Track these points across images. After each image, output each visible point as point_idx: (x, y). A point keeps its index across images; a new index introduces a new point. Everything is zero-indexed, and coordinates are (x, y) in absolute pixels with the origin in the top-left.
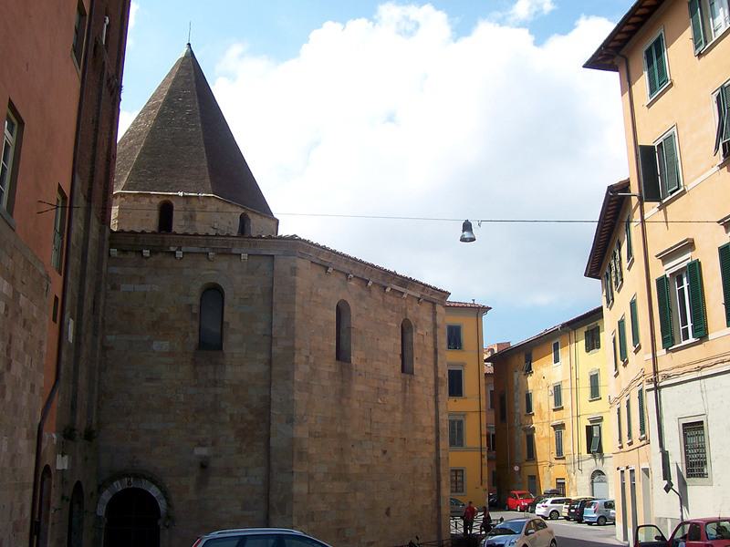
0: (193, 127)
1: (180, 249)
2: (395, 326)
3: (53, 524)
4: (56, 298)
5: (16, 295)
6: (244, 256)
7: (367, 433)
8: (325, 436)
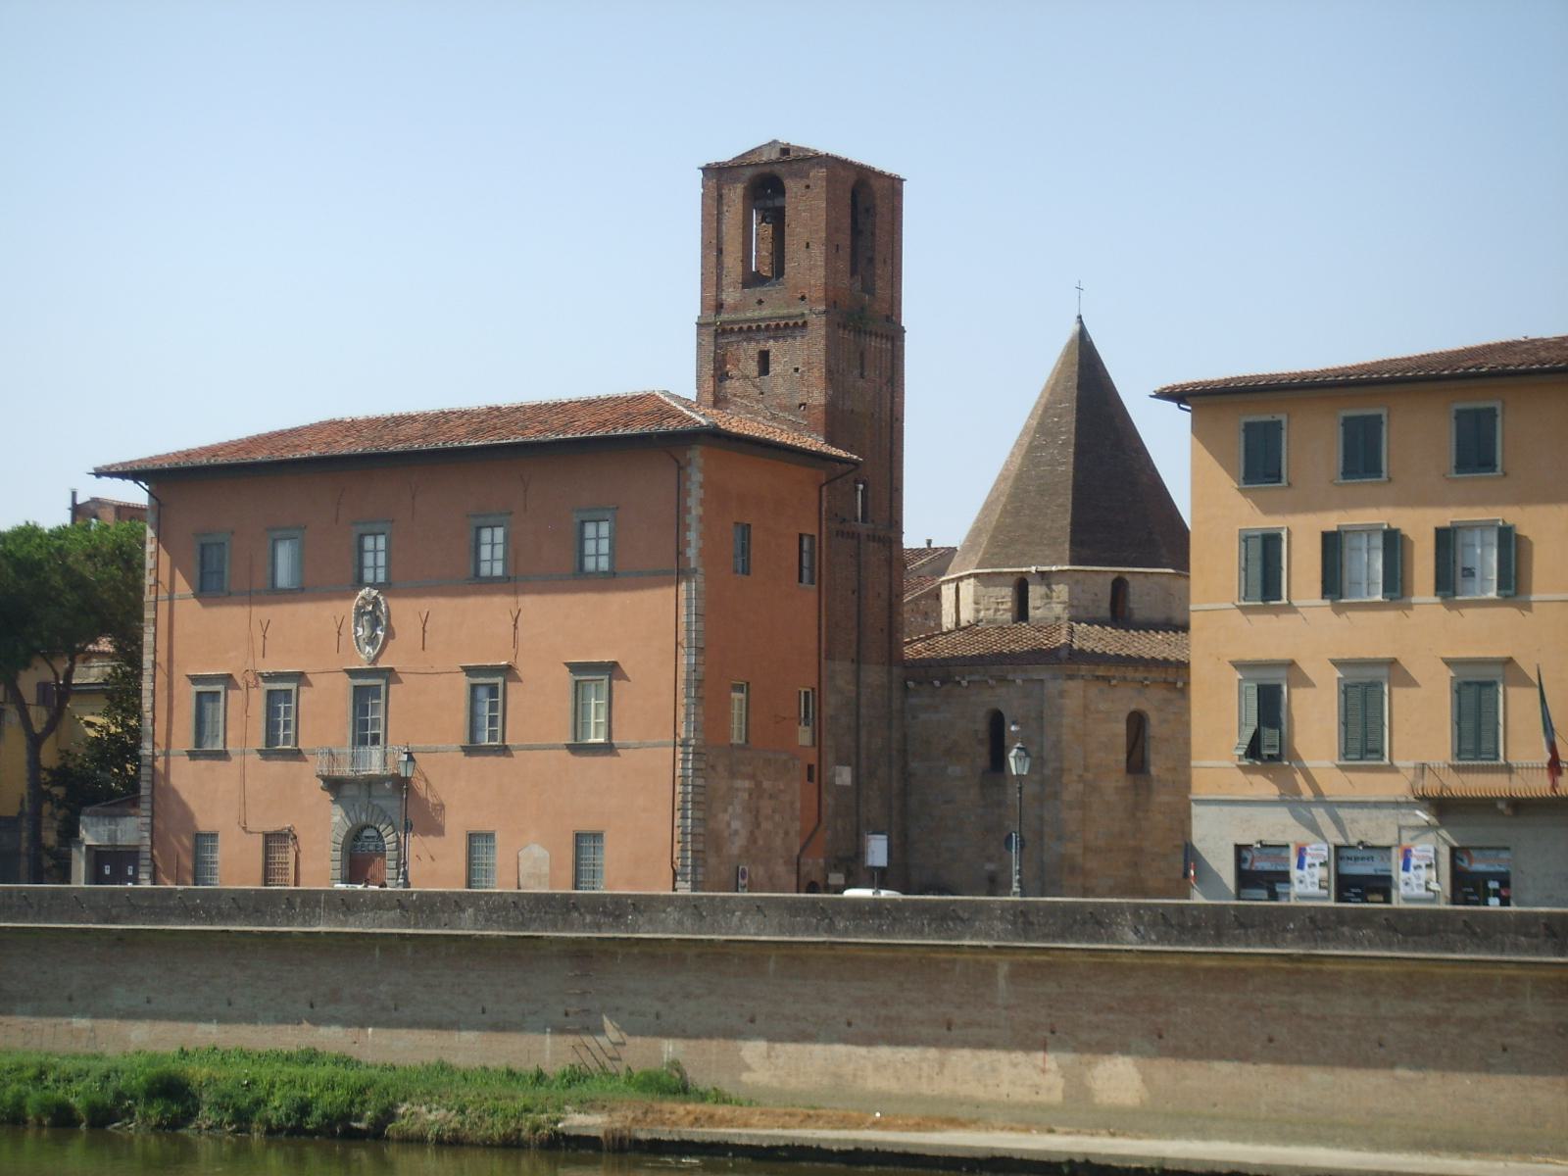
0: (1064, 463)
1: (964, 678)
3: (784, 1127)
4: (810, 768)
5: (758, 784)
6: (1019, 681)
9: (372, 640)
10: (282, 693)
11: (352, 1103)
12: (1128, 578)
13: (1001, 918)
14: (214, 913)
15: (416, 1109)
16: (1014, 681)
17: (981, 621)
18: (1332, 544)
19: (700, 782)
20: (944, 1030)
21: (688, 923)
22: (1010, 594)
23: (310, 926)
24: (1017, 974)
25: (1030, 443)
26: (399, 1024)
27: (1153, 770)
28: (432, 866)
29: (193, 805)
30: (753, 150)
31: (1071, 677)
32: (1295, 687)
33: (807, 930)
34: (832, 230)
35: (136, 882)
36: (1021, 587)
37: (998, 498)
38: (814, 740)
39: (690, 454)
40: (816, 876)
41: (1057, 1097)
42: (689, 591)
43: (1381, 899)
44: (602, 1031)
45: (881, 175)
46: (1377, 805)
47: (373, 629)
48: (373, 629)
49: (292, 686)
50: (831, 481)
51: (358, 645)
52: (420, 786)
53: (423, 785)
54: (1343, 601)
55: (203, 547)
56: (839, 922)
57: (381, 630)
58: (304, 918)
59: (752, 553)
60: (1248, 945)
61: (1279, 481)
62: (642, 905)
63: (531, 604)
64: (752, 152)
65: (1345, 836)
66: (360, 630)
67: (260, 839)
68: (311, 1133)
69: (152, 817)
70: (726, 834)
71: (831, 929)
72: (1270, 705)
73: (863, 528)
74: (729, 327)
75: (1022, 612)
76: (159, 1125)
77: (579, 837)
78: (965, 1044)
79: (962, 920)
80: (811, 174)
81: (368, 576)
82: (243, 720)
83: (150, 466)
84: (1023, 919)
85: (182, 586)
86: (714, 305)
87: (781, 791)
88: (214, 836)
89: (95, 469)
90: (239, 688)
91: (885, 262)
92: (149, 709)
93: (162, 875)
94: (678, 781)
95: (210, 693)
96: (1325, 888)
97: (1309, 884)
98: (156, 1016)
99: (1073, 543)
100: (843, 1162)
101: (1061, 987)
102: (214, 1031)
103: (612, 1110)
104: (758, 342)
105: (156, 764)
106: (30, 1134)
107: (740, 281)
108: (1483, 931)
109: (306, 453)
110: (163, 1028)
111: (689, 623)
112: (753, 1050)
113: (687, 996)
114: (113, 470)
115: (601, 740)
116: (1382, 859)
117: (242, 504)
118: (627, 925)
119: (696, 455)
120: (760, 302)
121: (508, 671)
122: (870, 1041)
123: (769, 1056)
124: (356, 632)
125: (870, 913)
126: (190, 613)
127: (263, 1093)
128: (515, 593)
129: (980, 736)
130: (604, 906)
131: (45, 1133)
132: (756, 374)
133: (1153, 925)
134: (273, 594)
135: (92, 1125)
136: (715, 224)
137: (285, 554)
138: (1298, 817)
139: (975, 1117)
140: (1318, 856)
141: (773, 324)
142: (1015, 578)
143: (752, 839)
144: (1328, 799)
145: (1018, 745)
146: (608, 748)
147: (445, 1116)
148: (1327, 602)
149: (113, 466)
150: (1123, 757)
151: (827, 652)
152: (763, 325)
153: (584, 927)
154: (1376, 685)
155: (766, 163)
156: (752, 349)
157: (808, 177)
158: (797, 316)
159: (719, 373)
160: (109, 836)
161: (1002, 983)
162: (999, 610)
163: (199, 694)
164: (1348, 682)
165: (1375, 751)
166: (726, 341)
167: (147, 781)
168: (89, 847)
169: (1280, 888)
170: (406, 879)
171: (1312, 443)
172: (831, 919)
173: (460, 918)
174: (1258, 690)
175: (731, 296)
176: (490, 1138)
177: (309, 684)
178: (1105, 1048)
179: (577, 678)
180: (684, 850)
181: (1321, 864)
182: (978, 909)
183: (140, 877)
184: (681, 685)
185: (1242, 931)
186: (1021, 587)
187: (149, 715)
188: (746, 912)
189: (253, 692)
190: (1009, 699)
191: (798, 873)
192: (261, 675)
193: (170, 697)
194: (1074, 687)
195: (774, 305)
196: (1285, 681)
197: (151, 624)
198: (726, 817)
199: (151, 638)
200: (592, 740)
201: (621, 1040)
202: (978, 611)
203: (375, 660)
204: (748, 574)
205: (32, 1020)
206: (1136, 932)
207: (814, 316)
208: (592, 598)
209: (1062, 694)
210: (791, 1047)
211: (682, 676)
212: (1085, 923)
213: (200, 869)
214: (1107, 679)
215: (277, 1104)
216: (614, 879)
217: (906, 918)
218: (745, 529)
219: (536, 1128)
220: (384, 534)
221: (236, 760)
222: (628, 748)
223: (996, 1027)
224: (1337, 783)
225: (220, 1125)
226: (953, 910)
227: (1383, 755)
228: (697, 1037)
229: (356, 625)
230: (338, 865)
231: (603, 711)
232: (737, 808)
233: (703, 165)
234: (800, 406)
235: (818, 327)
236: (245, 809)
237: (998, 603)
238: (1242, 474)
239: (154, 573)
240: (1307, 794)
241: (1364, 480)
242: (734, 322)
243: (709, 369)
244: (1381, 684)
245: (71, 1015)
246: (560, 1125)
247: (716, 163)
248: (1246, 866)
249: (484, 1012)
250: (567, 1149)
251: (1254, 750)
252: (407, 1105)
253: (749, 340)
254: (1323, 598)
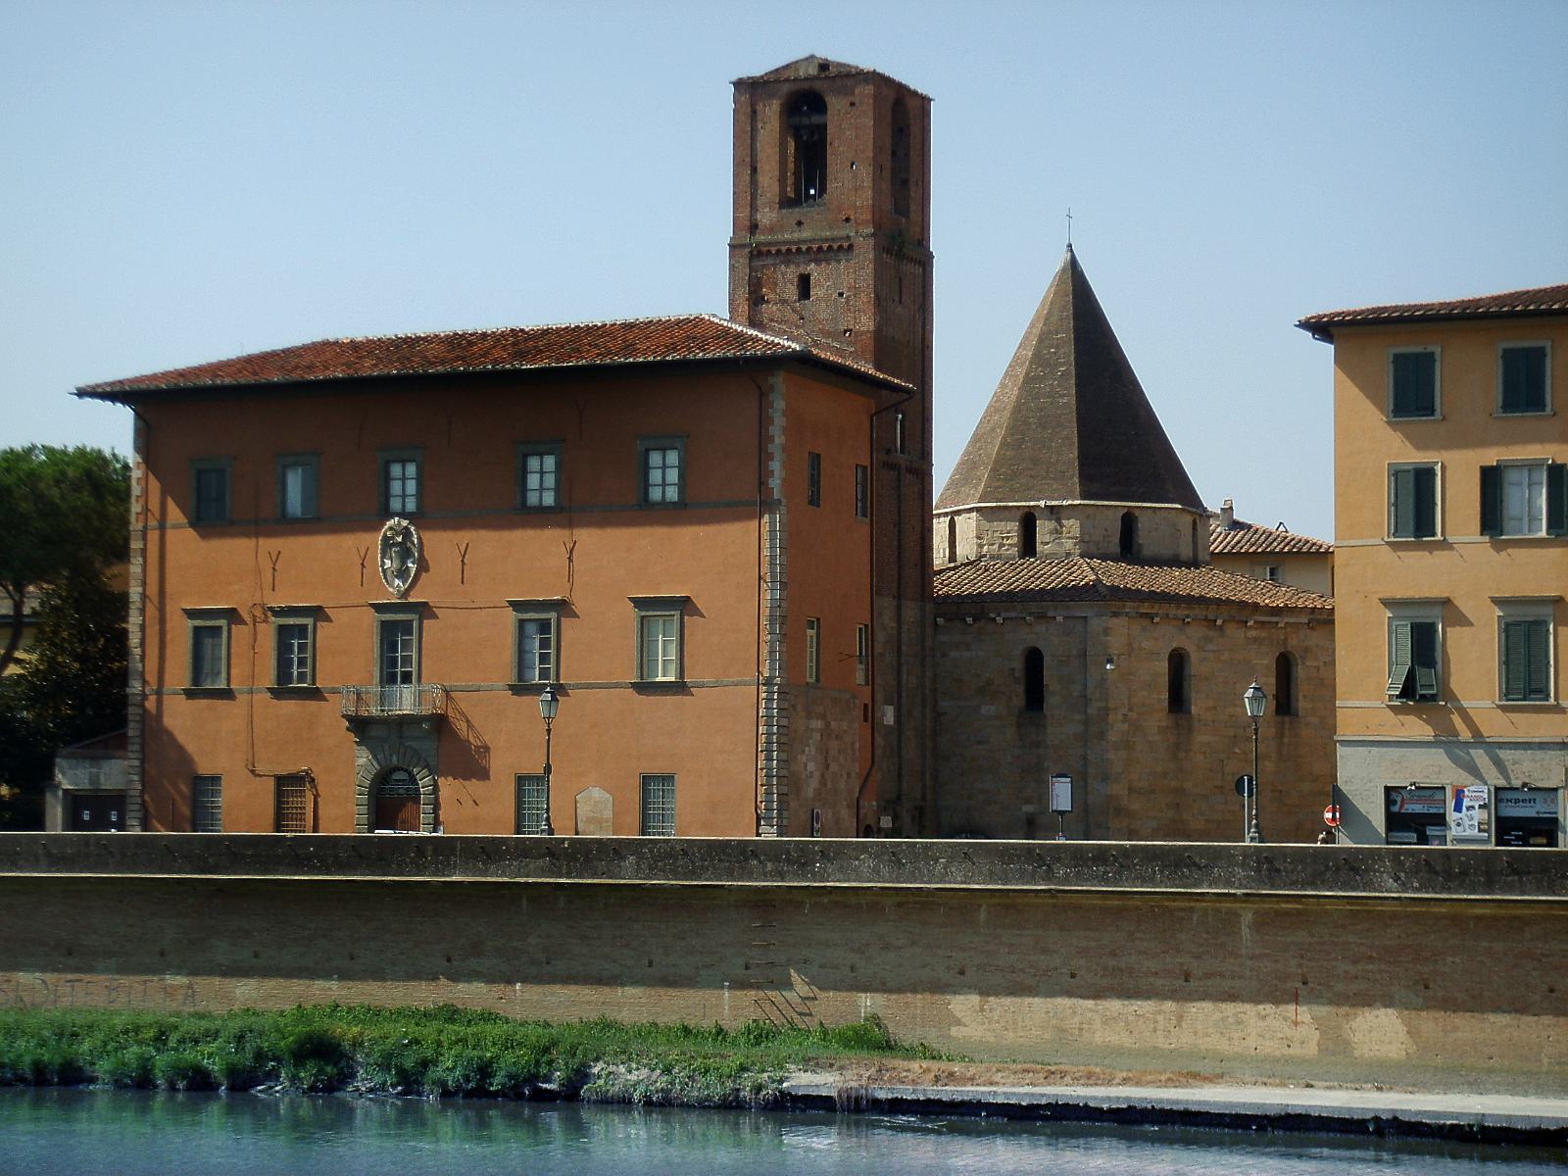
0: (1065, 395)
1: (999, 615)
2: (1266, 661)
4: (866, 705)
5: (828, 724)
6: (1059, 619)
7: (1216, 787)
8: (1153, 791)
9: (402, 573)
10: (295, 632)
11: (537, 1063)
12: (1137, 513)
13: (1243, 865)
14: (330, 862)
15: (612, 1068)
16: (1055, 618)
17: (985, 556)
18: (1492, 480)
19: (784, 722)
20: (1181, 982)
21: (885, 871)
22: (1016, 528)
23: (444, 875)
24: (1261, 924)
25: (1027, 374)
26: (553, 980)
27: (1194, 710)
28: (469, 810)
29: (191, 747)
30: (787, 65)
31: (1115, 615)
32: (1450, 626)
33: (1022, 879)
34: (878, 149)
35: (121, 826)
36: (1028, 522)
37: (993, 429)
38: (867, 677)
39: (772, 380)
40: (871, 821)
41: (1312, 1049)
42: (772, 523)
43: (1545, 841)
44: (788, 985)
45: (915, 93)
46: (1542, 746)
47: (403, 562)
48: (403, 562)
49: (309, 621)
50: (879, 412)
51: (385, 578)
52: (461, 727)
53: (464, 725)
54: (1503, 537)
55: (200, 473)
56: (1059, 869)
57: (413, 563)
58: (437, 867)
59: (822, 483)
60: (1523, 893)
61: (1432, 414)
62: (741, 855)
63: (587, 538)
64: (787, 66)
65: (1507, 778)
66: (388, 563)
67: (271, 784)
68: (495, 1095)
69: (143, 761)
70: (804, 776)
71: (1049, 877)
72: (1424, 645)
73: (902, 459)
74: (766, 249)
75: (1028, 546)
76: (313, 1088)
77: (646, 780)
78: (1206, 996)
79: (1199, 868)
80: (856, 92)
81: (395, 505)
82: (251, 657)
83: (143, 386)
84: (1268, 865)
85: (175, 513)
86: (747, 225)
87: (845, 732)
88: (215, 780)
89: (77, 389)
90: (245, 623)
91: (917, 185)
92: (138, 645)
93: (154, 821)
94: (762, 721)
95: (209, 630)
96: (1484, 831)
97: (1467, 826)
98: (265, 972)
99: (1082, 476)
100: (1114, 1121)
101: (1313, 936)
102: (335, 987)
103: (841, 1068)
104: (797, 265)
105: (147, 704)
106: (160, 1098)
107: (777, 201)
108: (1519, 871)
109: (330, 374)
110: (271, 985)
111: (773, 557)
112: (963, 1004)
113: (886, 947)
114: (100, 390)
115: (673, 679)
116: (1545, 801)
117: (263, 432)
118: (814, 874)
119: (779, 381)
120: (799, 223)
121: (563, 607)
122: (1098, 994)
123: (982, 1010)
124: (383, 564)
125: (1093, 859)
126: (185, 545)
127: (429, 1053)
128: (570, 524)
129: (1017, 675)
130: (788, 853)
131: (180, 1097)
132: (796, 297)
133: (1415, 871)
134: (284, 524)
135: (232, 1089)
136: (749, 141)
137: (294, 482)
138: (1457, 761)
139: (1219, 1071)
140: (1477, 798)
141: (815, 247)
142: (1021, 512)
143: (823, 782)
144: (1488, 740)
145: (1253, 685)
146: (680, 688)
147: (649, 1077)
148: (1487, 538)
149: (98, 386)
150: (1165, 696)
151: (875, 591)
152: (804, 248)
153: (765, 876)
154: (1541, 624)
155: (806, 79)
156: (790, 273)
157: (853, 94)
158: (841, 239)
159: (754, 296)
160: (90, 780)
161: (1245, 931)
162: (1004, 545)
163: (197, 629)
164: (1510, 620)
165: (1540, 691)
166: (762, 263)
167: (136, 721)
168: (66, 791)
169: (1431, 831)
170: (549, 825)
171: (1469, 377)
172: (1048, 866)
173: (620, 867)
174: (1412, 627)
175: (766, 216)
176: (708, 1098)
177: (328, 619)
178: (1365, 1000)
179: (643, 614)
180: (768, 793)
181: (1480, 807)
182: (1217, 855)
183: (128, 823)
184: (764, 622)
185: (1516, 878)
186: (1028, 522)
187: (138, 651)
188: (951, 859)
189: (261, 627)
190: (1051, 640)
191: (858, 818)
192: (271, 609)
193: (162, 633)
194: (1119, 624)
195: (813, 226)
196: (1440, 620)
197: (139, 553)
198: (804, 758)
199: (139, 570)
200: (660, 679)
201: (812, 995)
202: (981, 546)
203: (406, 593)
204: (818, 506)
205: (117, 977)
206: (1397, 879)
207: (861, 239)
208: (661, 532)
209: (1106, 631)
210: (1008, 1001)
211: (766, 612)
212: (1338, 869)
213: (201, 812)
214: (1150, 617)
215: (449, 1064)
216: (689, 821)
217: (1134, 865)
218: (815, 459)
219: (758, 1088)
220: (414, 461)
221: (242, 699)
222: (702, 686)
223: (1240, 977)
224: (1497, 724)
225: (383, 1087)
226: (1189, 856)
227: (1548, 695)
228: (899, 990)
229: (383, 557)
230: (364, 809)
231: (673, 650)
232: (811, 750)
233: (734, 79)
234: (845, 332)
235: (866, 252)
236: (248, 750)
237: (1003, 538)
238: (1391, 407)
239: (142, 501)
240: (1465, 735)
241: (1525, 414)
242: (769, 244)
243: (743, 292)
244: (1546, 623)
245: (163, 972)
246: (785, 1085)
247: (749, 78)
248: (1395, 809)
249: (650, 964)
250: (793, 1111)
251: (1408, 691)
252: (600, 1065)
253: (787, 263)
254: (1482, 535)
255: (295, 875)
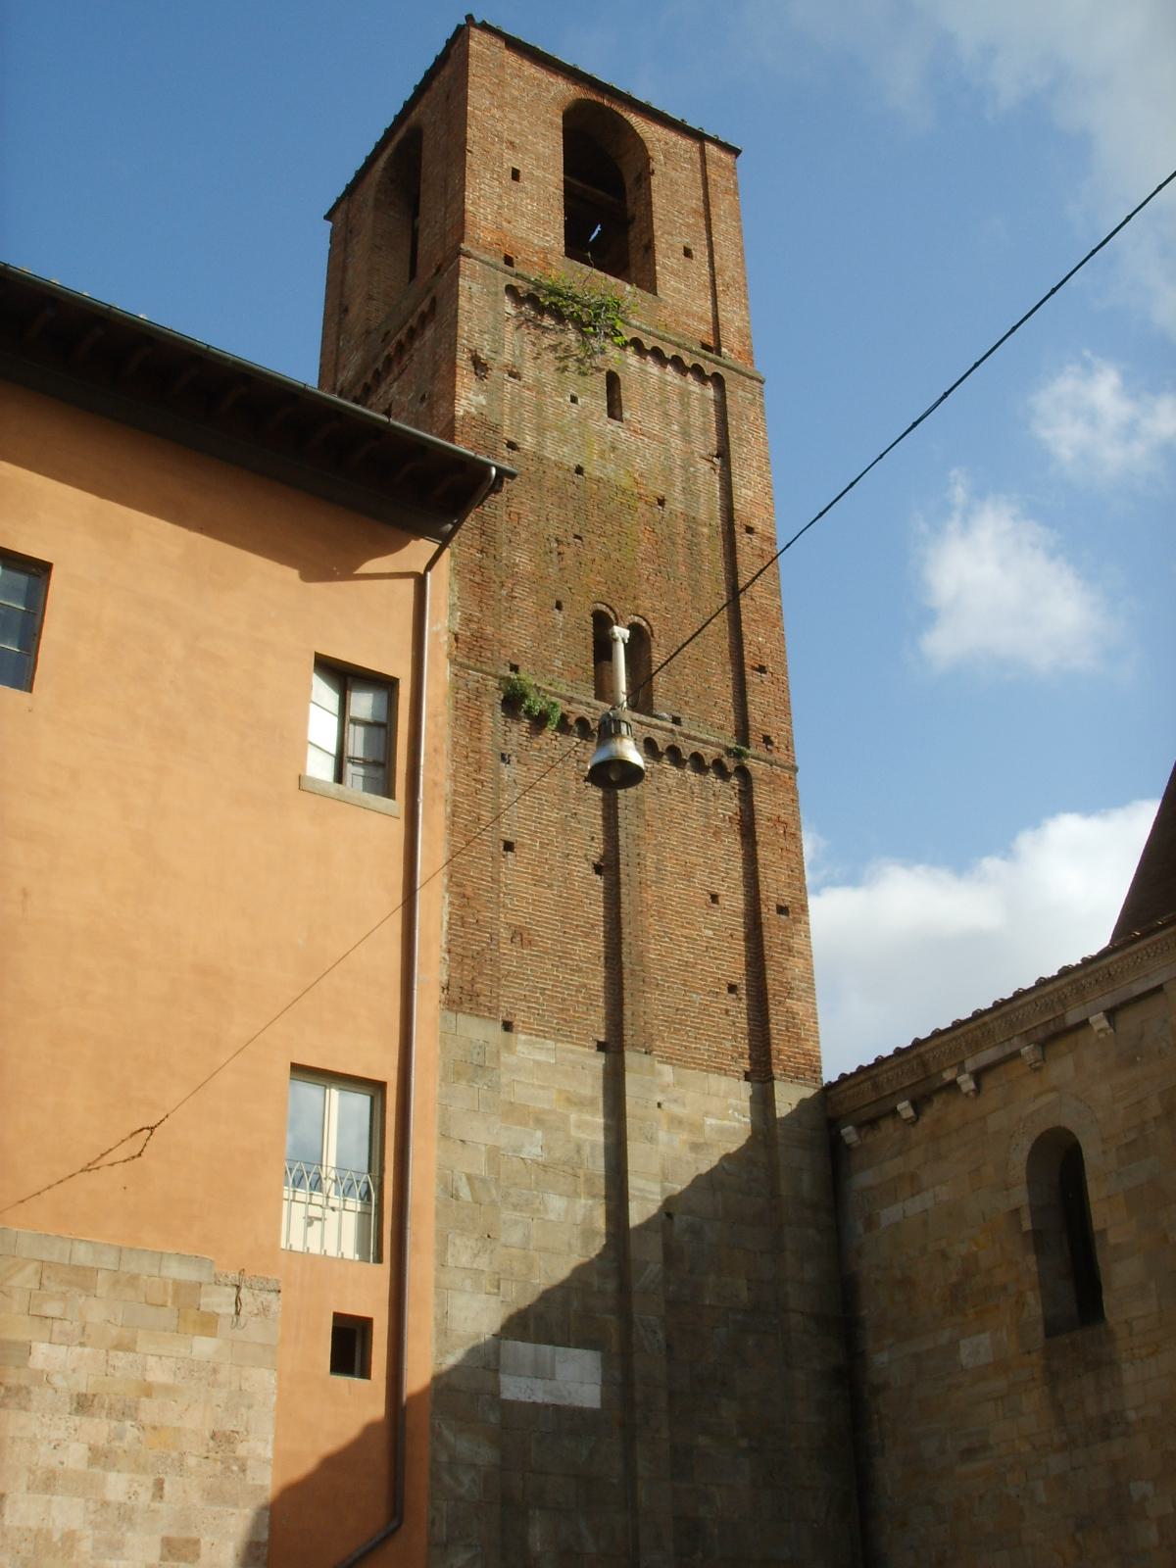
255: (8, 601)
